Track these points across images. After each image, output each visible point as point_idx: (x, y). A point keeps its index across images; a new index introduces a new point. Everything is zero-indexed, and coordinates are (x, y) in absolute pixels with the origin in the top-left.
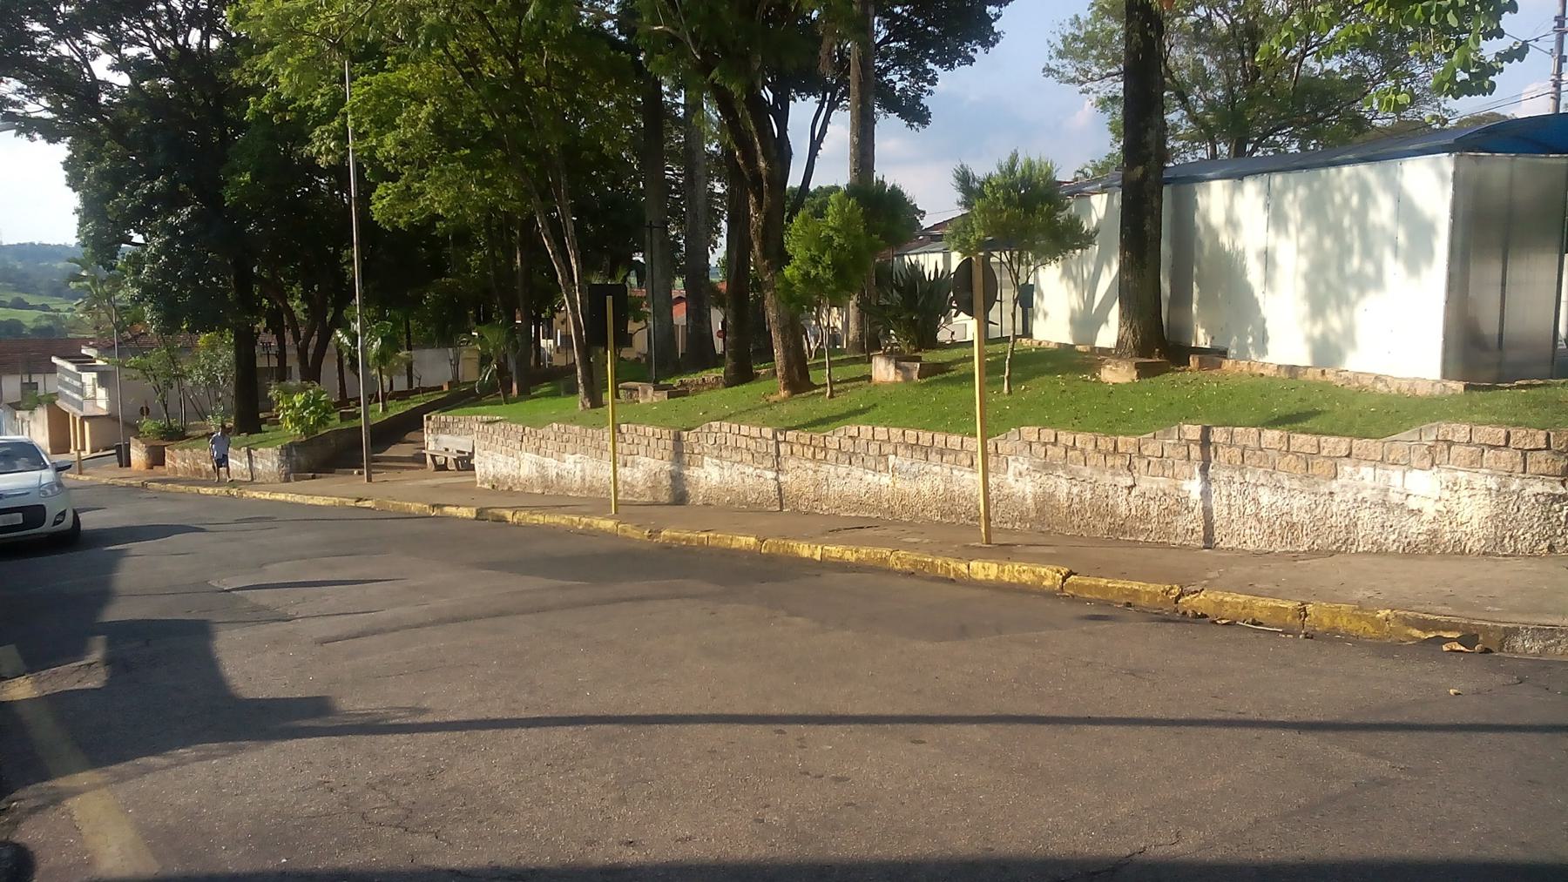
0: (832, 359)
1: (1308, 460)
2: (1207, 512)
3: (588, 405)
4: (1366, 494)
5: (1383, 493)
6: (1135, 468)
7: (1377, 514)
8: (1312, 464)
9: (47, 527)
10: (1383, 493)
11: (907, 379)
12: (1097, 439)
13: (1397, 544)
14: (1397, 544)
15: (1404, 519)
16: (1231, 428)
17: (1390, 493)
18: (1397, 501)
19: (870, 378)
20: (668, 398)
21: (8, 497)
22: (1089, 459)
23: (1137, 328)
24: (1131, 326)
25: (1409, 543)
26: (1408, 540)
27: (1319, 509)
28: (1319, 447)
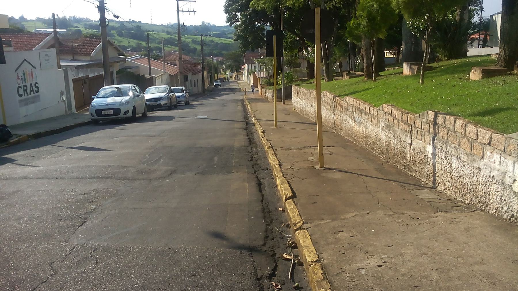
0: (422, 62)
1: (472, 143)
2: (434, 165)
3: (327, 80)
4: (495, 173)
5: (503, 175)
6: (413, 134)
7: (499, 189)
8: (474, 146)
9: (121, 115)
10: (503, 175)
11: (413, 73)
12: (402, 114)
13: (507, 214)
14: (507, 214)
15: (511, 197)
16: (445, 116)
17: (507, 177)
18: (508, 184)
19: (402, 73)
20: (350, 78)
21: (109, 105)
22: (400, 125)
23: (507, 50)
24: (504, 49)
25: (513, 216)
26: (512, 213)
27: (475, 178)
28: (477, 135)
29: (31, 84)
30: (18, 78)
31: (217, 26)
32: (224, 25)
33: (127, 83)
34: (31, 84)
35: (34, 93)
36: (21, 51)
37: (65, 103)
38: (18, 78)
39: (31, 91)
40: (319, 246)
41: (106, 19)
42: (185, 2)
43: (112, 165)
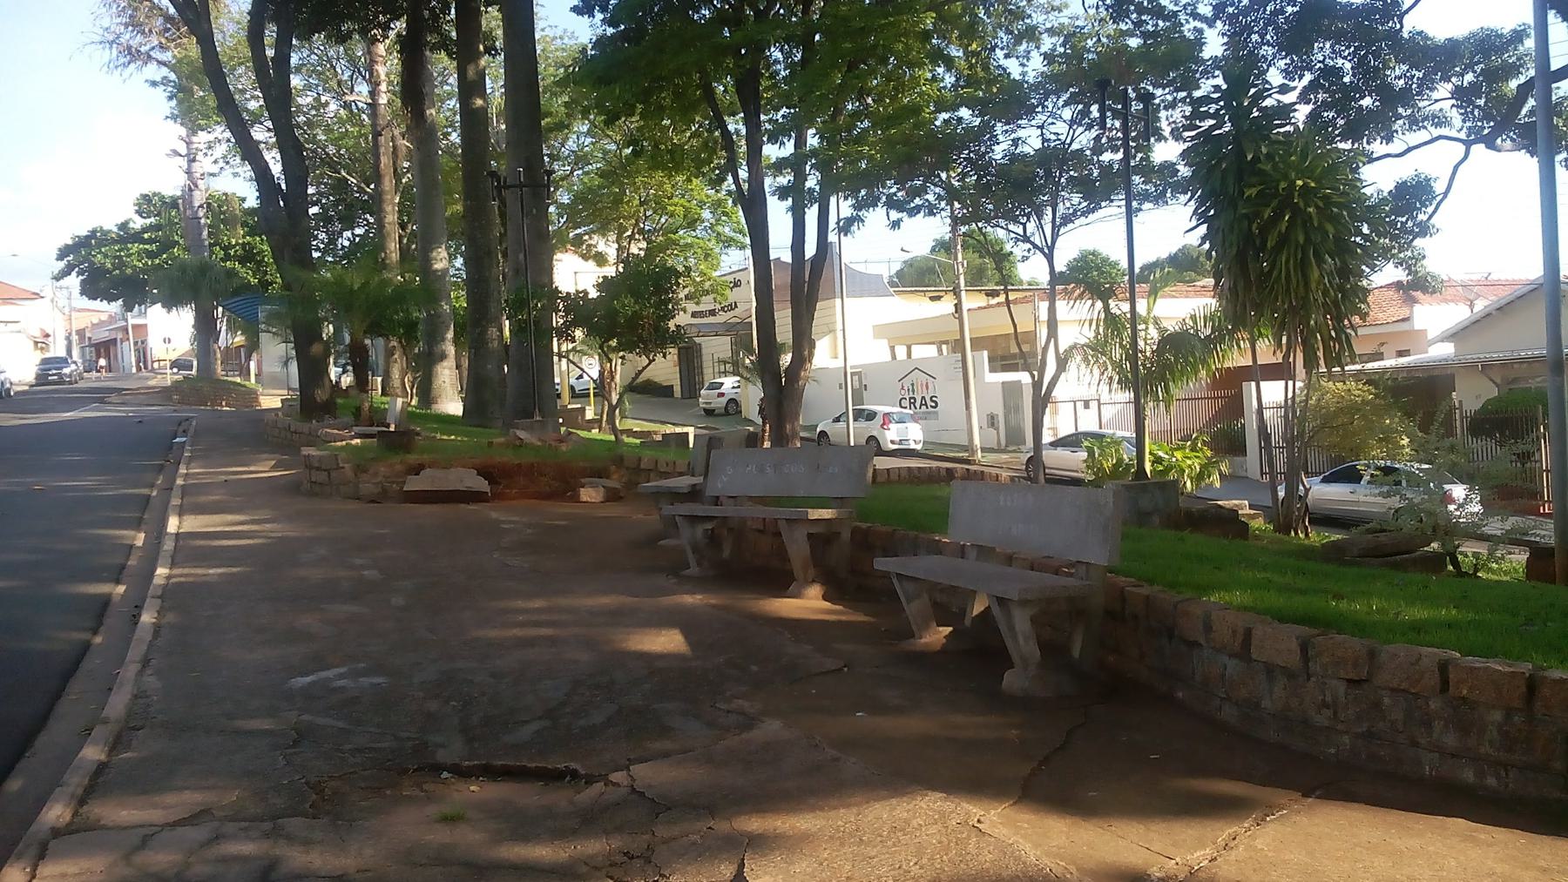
29: (923, 398)
30: (902, 389)
31: (1483, 145)
32: (1489, 151)
33: (200, 365)
34: (923, 398)
35: (927, 408)
36: (1507, 280)
37: (998, 433)
38: (902, 389)
39: (921, 405)
40: (1445, 684)
41: (747, 169)
42: (9, 324)
43: (1554, 562)
